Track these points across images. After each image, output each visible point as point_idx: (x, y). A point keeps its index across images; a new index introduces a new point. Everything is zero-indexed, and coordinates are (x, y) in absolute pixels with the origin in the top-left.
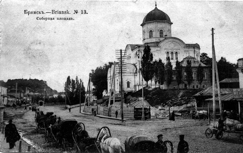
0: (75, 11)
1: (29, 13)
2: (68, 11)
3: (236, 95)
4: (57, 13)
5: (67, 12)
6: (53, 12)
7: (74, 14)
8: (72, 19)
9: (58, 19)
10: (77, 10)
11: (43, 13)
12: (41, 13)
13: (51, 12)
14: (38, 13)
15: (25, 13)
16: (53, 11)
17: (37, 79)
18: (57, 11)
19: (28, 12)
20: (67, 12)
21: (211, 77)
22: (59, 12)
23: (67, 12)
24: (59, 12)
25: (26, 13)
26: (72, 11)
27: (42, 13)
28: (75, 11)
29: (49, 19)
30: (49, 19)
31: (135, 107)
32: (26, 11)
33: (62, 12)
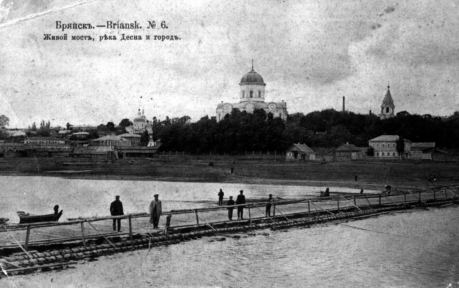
0: (150, 22)
1: (65, 27)
2: (137, 23)
3: (434, 194)
4: (116, 27)
5: (134, 26)
6: (111, 25)
7: (148, 28)
8: (176, 38)
9: (74, 38)
10: (154, 22)
11: (90, 26)
12: (86, 26)
13: (106, 25)
14: (80, 27)
15: (57, 28)
16: (109, 23)
17: (122, 122)
18: (117, 23)
19: (63, 25)
20: (134, 26)
21: (52, 170)
22: (119, 26)
23: (135, 26)
24: (119, 26)
25: (59, 26)
26: (144, 24)
27: (88, 27)
28: (150, 22)
29: (168, 37)
30: (168, 37)
31: (232, 172)
32: (59, 23)
33: (126, 25)
